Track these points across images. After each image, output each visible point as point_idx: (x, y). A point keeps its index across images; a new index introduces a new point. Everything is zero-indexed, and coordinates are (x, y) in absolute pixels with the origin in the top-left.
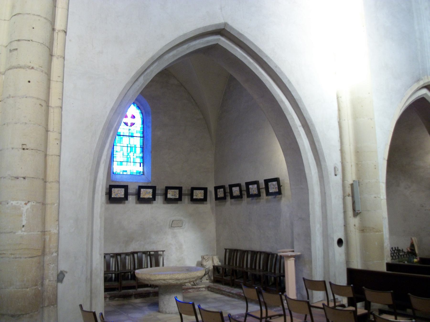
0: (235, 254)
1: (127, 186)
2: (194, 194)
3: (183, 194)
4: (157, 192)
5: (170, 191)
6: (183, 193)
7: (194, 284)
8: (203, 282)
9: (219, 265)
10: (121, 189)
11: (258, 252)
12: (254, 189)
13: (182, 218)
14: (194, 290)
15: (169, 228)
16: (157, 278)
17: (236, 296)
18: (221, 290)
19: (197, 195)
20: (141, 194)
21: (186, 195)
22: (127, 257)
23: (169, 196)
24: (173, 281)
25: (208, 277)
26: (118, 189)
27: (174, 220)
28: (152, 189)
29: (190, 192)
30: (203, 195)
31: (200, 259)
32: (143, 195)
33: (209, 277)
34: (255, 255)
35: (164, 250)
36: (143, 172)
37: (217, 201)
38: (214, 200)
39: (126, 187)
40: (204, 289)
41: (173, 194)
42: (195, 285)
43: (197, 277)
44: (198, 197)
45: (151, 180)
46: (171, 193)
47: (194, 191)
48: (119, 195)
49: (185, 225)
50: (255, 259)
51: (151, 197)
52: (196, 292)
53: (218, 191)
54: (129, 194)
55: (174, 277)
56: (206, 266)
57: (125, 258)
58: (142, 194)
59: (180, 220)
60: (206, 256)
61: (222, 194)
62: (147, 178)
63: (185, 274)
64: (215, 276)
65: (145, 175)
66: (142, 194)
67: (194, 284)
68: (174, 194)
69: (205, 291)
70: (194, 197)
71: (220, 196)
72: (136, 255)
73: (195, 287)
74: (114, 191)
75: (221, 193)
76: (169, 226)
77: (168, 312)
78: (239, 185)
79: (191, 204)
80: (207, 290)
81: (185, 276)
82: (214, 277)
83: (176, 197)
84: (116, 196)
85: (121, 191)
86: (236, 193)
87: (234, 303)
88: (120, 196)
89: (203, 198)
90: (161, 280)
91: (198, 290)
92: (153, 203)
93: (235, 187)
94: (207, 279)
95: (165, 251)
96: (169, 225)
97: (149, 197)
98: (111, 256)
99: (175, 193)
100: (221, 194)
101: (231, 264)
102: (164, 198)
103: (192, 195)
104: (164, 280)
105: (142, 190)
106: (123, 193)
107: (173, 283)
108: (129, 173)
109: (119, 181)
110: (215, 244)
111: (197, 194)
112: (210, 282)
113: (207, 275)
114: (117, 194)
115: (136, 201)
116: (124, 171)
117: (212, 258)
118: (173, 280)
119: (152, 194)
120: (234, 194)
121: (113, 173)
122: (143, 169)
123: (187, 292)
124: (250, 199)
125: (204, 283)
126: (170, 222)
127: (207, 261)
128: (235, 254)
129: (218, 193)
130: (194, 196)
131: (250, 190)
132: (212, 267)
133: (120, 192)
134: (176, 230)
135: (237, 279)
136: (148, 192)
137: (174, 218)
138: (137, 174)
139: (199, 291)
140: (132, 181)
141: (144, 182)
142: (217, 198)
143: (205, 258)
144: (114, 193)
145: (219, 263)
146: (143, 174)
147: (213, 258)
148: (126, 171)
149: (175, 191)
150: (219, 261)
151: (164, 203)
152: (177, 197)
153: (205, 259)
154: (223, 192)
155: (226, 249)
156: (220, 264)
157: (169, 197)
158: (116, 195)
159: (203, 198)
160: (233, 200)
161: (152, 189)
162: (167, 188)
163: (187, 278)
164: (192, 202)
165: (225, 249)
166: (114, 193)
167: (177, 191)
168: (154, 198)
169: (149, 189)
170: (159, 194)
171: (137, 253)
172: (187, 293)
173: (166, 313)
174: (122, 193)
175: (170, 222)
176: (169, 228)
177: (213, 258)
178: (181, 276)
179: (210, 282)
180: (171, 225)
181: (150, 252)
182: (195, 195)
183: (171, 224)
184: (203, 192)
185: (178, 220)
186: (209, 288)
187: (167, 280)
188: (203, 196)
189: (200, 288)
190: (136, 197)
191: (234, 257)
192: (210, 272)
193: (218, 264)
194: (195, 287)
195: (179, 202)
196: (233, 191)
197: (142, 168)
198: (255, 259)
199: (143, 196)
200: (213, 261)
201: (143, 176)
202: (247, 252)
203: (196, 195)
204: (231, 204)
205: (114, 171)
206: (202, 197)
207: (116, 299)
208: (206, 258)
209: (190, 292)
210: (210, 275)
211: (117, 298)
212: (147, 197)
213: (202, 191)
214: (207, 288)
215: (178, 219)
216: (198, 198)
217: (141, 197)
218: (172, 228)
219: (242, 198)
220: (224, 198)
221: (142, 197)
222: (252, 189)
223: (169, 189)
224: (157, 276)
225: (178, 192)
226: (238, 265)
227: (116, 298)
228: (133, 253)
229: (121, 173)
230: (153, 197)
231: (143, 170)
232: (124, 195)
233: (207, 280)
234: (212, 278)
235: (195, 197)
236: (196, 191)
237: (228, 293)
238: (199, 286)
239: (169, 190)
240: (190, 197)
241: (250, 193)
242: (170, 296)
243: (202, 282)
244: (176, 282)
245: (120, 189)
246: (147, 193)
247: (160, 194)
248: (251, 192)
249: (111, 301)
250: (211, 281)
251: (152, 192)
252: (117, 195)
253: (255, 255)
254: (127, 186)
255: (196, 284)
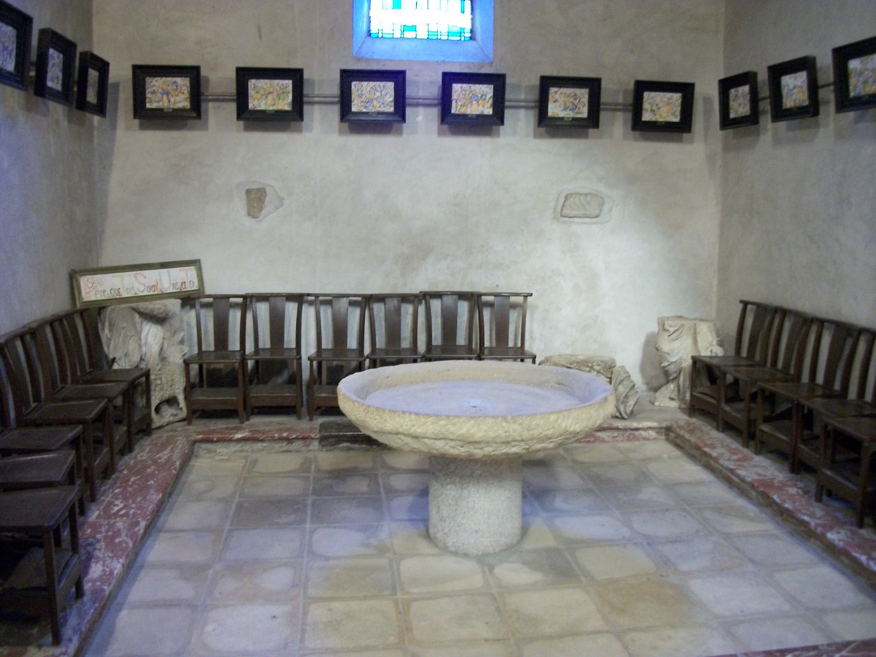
0: (777, 322)
1: (402, 73)
2: (646, 106)
3: (605, 104)
4: (509, 95)
5: (556, 93)
6: (602, 100)
7: (618, 414)
8: (657, 404)
9: (716, 357)
10: (382, 84)
11: (861, 331)
12: (867, 73)
13: (600, 188)
14: (616, 434)
15: (554, 218)
16: (388, 425)
17: (753, 494)
18: (705, 454)
19: (655, 108)
20: (454, 102)
21: (614, 108)
22: (407, 310)
23: (554, 109)
24: (453, 447)
25: (676, 392)
26: (372, 84)
27: (572, 194)
28: (492, 86)
29: (630, 100)
30: (679, 109)
31: (654, 328)
32: (460, 103)
33: (679, 390)
34: (850, 342)
35: (527, 291)
36: (472, 31)
37: (730, 132)
38: (718, 127)
39: (398, 77)
40: (652, 434)
41: (568, 104)
42: (623, 418)
43: (561, 435)
44: (661, 116)
45: (491, 56)
46: (561, 100)
47: (646, 95)
48: (375, 103)
49: (611, 210)
50: (846, 352)
51: (489, 111)
52: (622, 441)
53: (731, 96)
54: (408, 101)
55: (452, 429)
56: (668, 354)
57: (398, 311)
58: (456, 102)
59: (592, 195)
60: (671, 323)
61: (745, 105)
62: (481, 48)
63: (504, 424)
64: (695, 394)
65: (477, 41)
66: (456, 102)
67: (621, 414)
68: (572, 103)
69: (655, 439)
70: (646, 117)
71: (736, 112)
72: (436, 305)
73: (620, 424)
74: (358, 90)
75: (741, 100)
76: (554, 212)
77: (453, 549)
78: (805, 64)
79: (636, 139)
80: (663, 437)
81: (501, 433)
82: (692, 396)
83: (577, 113)
84: (366, 107)
85: (382, 91)
86: (794, 97)
87: (738, 526)
88: (380, 107)
89: (677, 119)
90: (402, 437)
91: (631, 437)
92: (498, 135)
93: (792, 75)
94: (673, 396)
95: (531, 295)
96: (555, 209)
97: (482, 112)
98: (352, 304)
99: (575, 99)
100: (740, 105)
101: (757, 357)
102: (537, 118)
103: (637, 107)
104: (416, 437)
105: (457, 88)
106: (390, 97)
107: (454, 452)
108: (422, 34)
109: (381, 58)
110: (715, 282)
111: (657, 105)
112: (680, 408)
113: (672, 382)
114: (370, 101)
115: (438, 125)
116: (405, 28)
117: (692, 332)
118: (452, 444)
119: (491, 101)
120: (789, 103)
121: (369, 34)
122: (473, 20)
123: (591, 439)
124: (851, 115)
125: (661, 410)
126: (557, 200)
127: (675, 340)
128: (777, 322)
129: (731, 103)
130: (643, 112)
131: (853, 81)
132: (687, 363)
133: (378, 94)
134: (578, 227)
135: (767, 420)
136: (480, 96)
137: (570, 187)
138: (450, 38)
139: (636, 438)
140: (425, 58)
141: (468, 63)
142: (727, 122)
143: (667, 327)
144: (360, 96)
145: (714, 351)
146: (472, 38)
147: (695, 330)
148: (414, 28)
149: (575, 95)
150: (715, 343)
151: (537, 136)
152: (584, 113)
153: (668, 331)
154: (748, 96)
155: (745, 304)
156: (719, 351)
157: (554, 113)
158: (365, 104)
159: (677, 119)
160: (782, 125)
161: (492, 86)
162: (547, 83)
163: (514, 441)
164: (637, 133)
165: (741, 301)
166: (359, 96)
167: (583, 94)
168: (498, 117)
169: (481, 86)
170: (520, 101)
171: (438, 295)
172: (588, 442)
173: (445, 550)
174: (388, 96)
175: (557, 200)
176: (554, 218)
177: (698, 331)
178: (484, 428)
179: (680, 408)
180: (562, 211)
181: (480, 295)
182: (649, 109)
183: (560, 207)
184: (677, 100)
185: (586, 194)
186: (668, 432)
187: (426, 441)
188: (678, 113)
189: (637, 429)
190: (438, 110)
191: (768, 336)
192: (684, 376)
193: (711, 351)
194: (620, 424)
195: (591, 131)
196: (785, 92)
197: (470, 16)
198: (846, 352)
199: (459, 107)
200: (695, 341)
201: (472, 43)
202: (822, 323)
203: (652, 111)
204: (777, 141)
205: (374, 30)
206: (676, 117)
207: (345, 444)
208: (672, 330)
209: (603, 441)
210: (681, 387)
211: (347, 441)
212: (474, 113)
213: (677, 97)
214: (663, 430)
215: (586, 191)
216: (661, 120)
217: (453, 111)
218: (566, 219)
219: (816, 113)
220: (752, 119)
221: (457, 112)
222: (861, 73)
223: (555, 85)
224: (387, 416)
225: (587, 96)
226: (780, 365)
227: (343, 441)
228: (426, 297)
229: (397, 35)
230: (494, 111)
231: (473, 25)
232: (393, 104)
233: (672, 399)
234: (688, 396)
235: (646, 117)
236: (653, 94)
237: (726, 471)
238: (635, 425)
239: (552, 90)
240: (629, 116)
241: (852, 94)
242: (462, 489)
243: (653, 403)
244: (463, 450)
245: (378, 83)
246: (474, 97)
247: (523, 104)
248: (855, 87)
249: (327, 451)
250: (683, 406)
251: (491, 94)
252: (369, 104)
253: (850, 342)
254: (402, 73)
255: (626, 417)
